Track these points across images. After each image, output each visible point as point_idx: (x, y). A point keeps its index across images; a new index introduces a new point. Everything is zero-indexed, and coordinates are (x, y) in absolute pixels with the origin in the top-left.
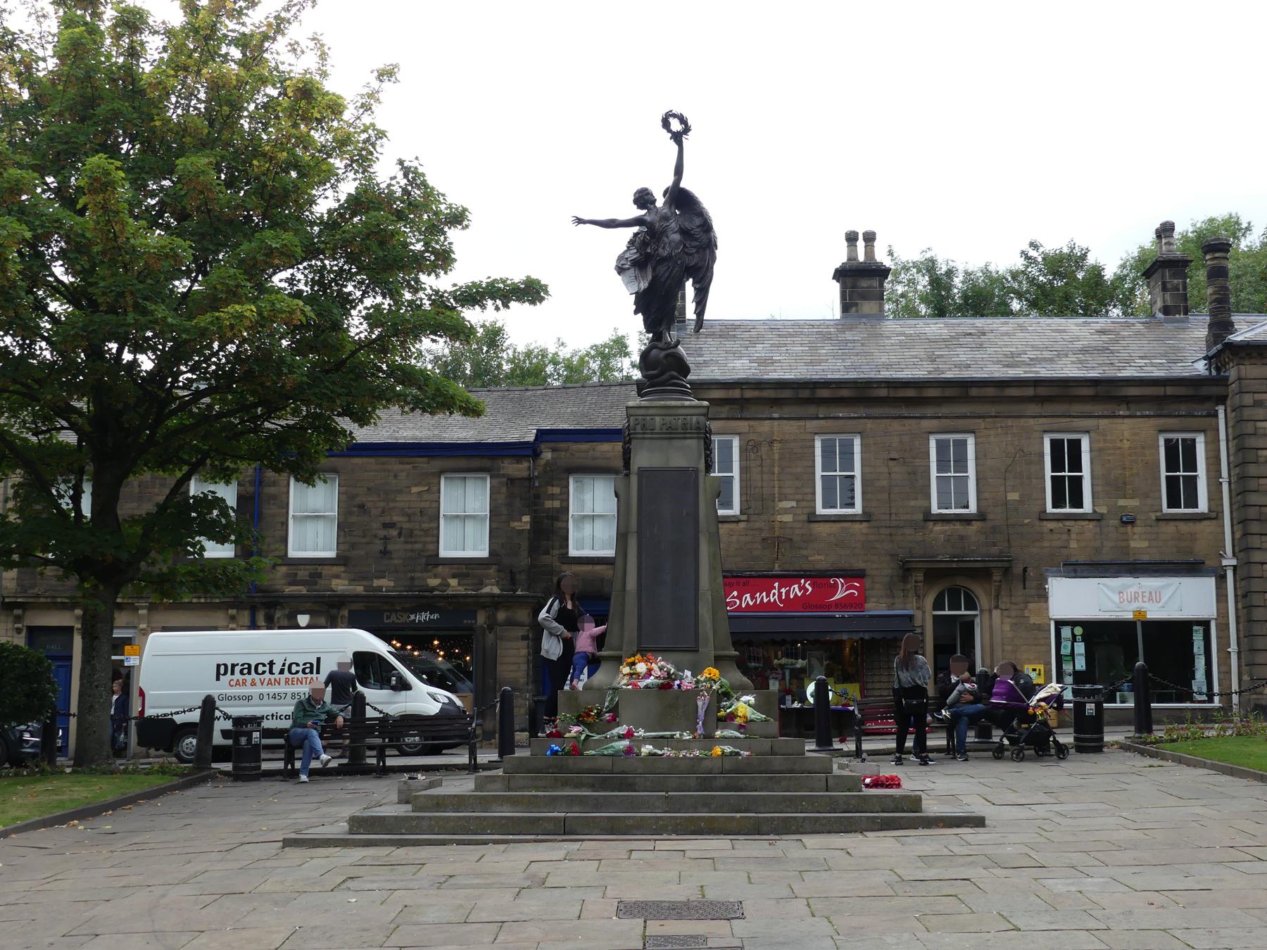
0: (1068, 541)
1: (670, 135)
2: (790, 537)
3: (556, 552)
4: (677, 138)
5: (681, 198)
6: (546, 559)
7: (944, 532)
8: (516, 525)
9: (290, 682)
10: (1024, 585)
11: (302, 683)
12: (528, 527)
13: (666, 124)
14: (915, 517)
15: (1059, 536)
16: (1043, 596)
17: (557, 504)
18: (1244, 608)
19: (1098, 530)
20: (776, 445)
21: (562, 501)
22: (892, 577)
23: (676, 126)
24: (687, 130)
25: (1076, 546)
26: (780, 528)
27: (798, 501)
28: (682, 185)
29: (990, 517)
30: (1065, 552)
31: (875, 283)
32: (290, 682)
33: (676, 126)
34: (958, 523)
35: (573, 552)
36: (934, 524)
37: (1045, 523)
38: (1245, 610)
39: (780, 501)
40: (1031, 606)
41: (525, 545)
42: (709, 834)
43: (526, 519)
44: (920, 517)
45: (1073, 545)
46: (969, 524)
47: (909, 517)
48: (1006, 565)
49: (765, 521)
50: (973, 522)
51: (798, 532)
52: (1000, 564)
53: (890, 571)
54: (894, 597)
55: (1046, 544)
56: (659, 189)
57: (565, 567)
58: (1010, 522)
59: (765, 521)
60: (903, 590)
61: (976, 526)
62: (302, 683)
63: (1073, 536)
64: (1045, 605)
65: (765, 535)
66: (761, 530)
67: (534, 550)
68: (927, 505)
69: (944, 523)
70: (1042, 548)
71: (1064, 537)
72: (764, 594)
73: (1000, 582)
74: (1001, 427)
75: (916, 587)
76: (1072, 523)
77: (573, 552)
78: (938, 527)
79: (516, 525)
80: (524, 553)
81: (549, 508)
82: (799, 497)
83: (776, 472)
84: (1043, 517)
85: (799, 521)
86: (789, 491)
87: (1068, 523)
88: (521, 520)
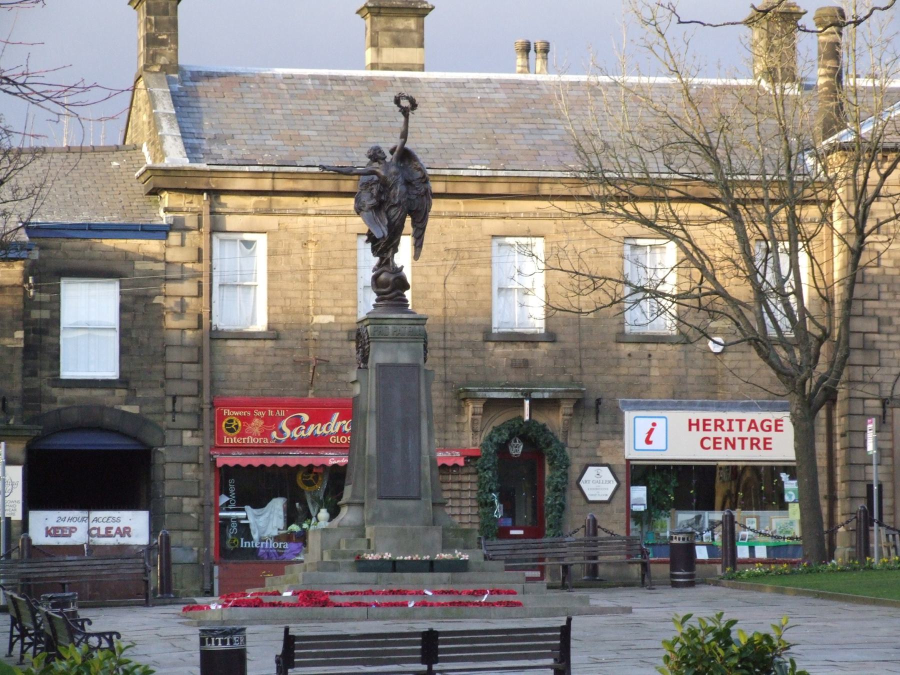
0: (649, 368)
1: (399, 109)
2: (326, 359)
3: (45, 373)
4: (405, 112)
5: (405, 156)
6: (35, 383)
7: (506, 355)
8: (7, 342)
9: (761, 445)
10: (597, 419)
11: (733, 447)
12: (22, 345)
13: (397, 101)
14: (473, 338)
15: (638, 362)
16: (618, 431)
17: (46, 314)
18: (842, 449)
19: (682, 355)
20: (311, 246)
21: (52, 311)
22: (446, 407)
23: (405, 103)
24: (414, 105)
25: (658, 374)
26: (315, 348)
27: (337, 315)
28: (406, 146)
29: (561, 337)
30: (644, 380)
31: (412, 23)
32: (761, 445)
33: (405, 103)
34: (522, 345)
35: (66, 373)
36: (495, 346)
37: (623, 345)
38: (844, 451)
39: (316, 314)
40: (604, 443)
41: (18, 364)
42: (667, 467)
43: (20, 334)
44: (479, 337)
45: (655, 372)
46: (536, 347)
47: (465, 337)
48: (578, 396)
49: (297, 339)
50: (540, 344)
51: (336, 352)
52: (571, 395)
53: (442, 401)
54: (445, 432)
55: (624, 371)
56: (389, 142)
57: (55, 392)
58: (585, 344)
59: (297, 339)
60: (458, 423)
61: (544, 347)
62: (733, 447)
63: (654, 362)
64: (620, 443)
65: (297, 355)
66: (292, 349)
67: (30, 372)
68: (488, 323)
69: (507, 345)
70: (618, 376)
71: (645, 363)
72: (319, 425)
73: (570, 415)
74: (575, 231)
75: (473, 420)
76: (653, 346)
77: (66, 373)
78: (499, 350)
79: (7, 342)
80: (17, 377)
81: (37, 320)
82: (339, 310)
83: (311, 280)
84: (621, 338)
85: (337, 340)
86: (325, 303)
87: (649, 347)
88: (12, 336)
